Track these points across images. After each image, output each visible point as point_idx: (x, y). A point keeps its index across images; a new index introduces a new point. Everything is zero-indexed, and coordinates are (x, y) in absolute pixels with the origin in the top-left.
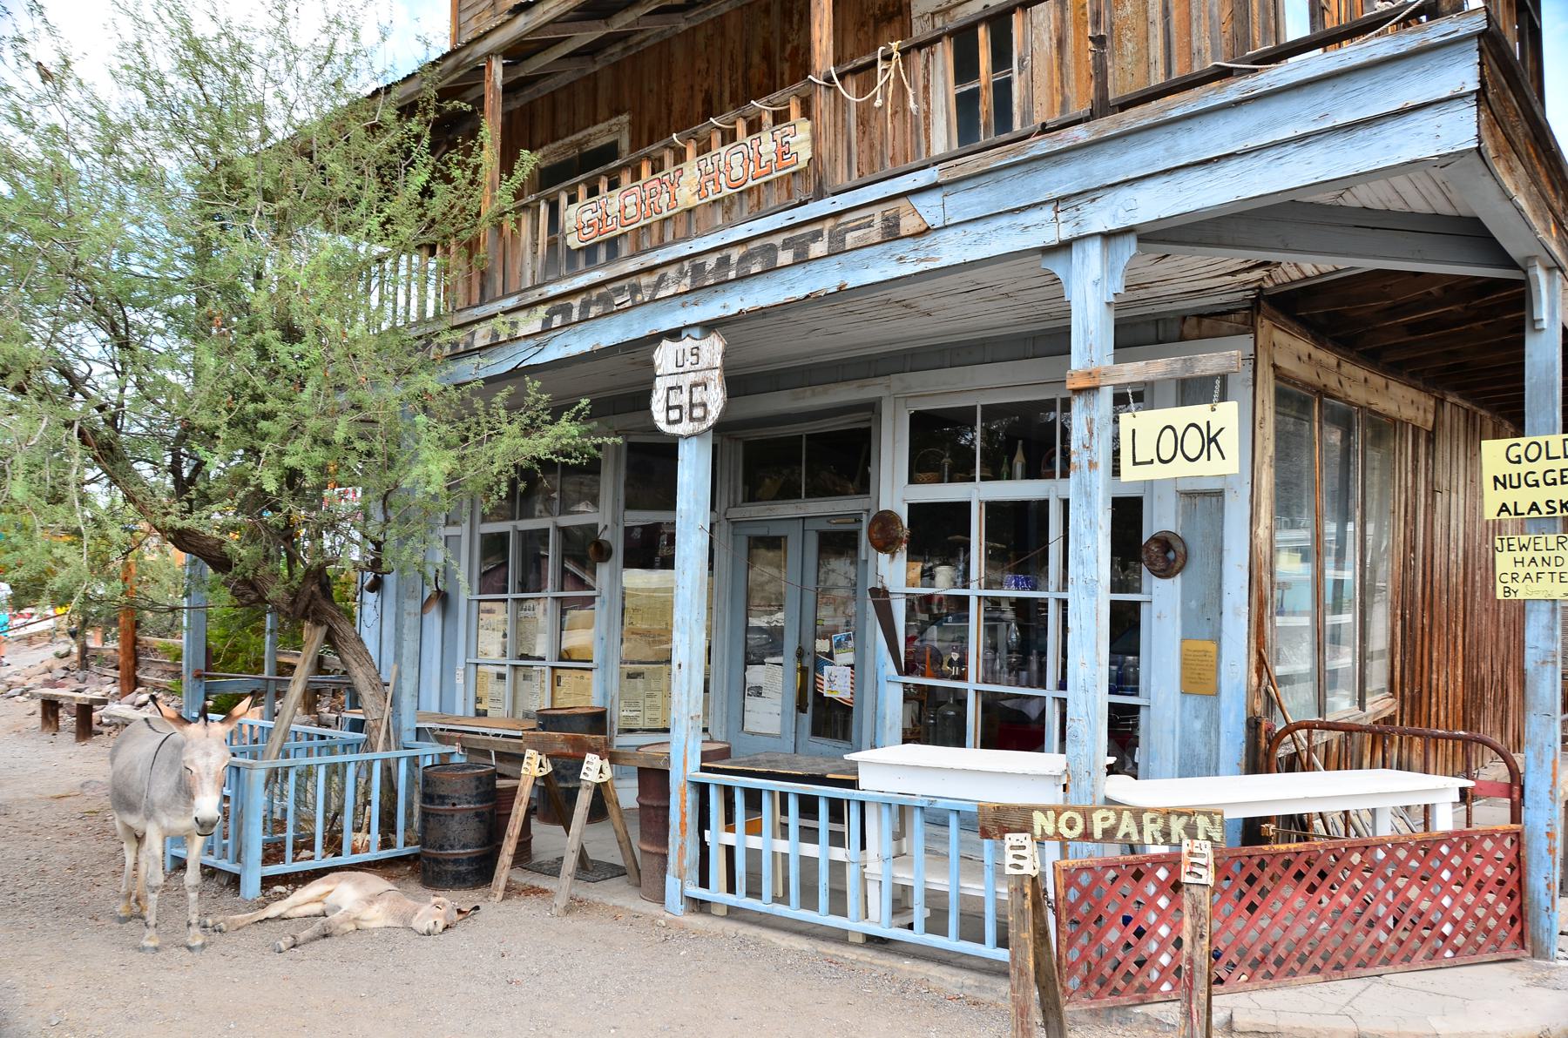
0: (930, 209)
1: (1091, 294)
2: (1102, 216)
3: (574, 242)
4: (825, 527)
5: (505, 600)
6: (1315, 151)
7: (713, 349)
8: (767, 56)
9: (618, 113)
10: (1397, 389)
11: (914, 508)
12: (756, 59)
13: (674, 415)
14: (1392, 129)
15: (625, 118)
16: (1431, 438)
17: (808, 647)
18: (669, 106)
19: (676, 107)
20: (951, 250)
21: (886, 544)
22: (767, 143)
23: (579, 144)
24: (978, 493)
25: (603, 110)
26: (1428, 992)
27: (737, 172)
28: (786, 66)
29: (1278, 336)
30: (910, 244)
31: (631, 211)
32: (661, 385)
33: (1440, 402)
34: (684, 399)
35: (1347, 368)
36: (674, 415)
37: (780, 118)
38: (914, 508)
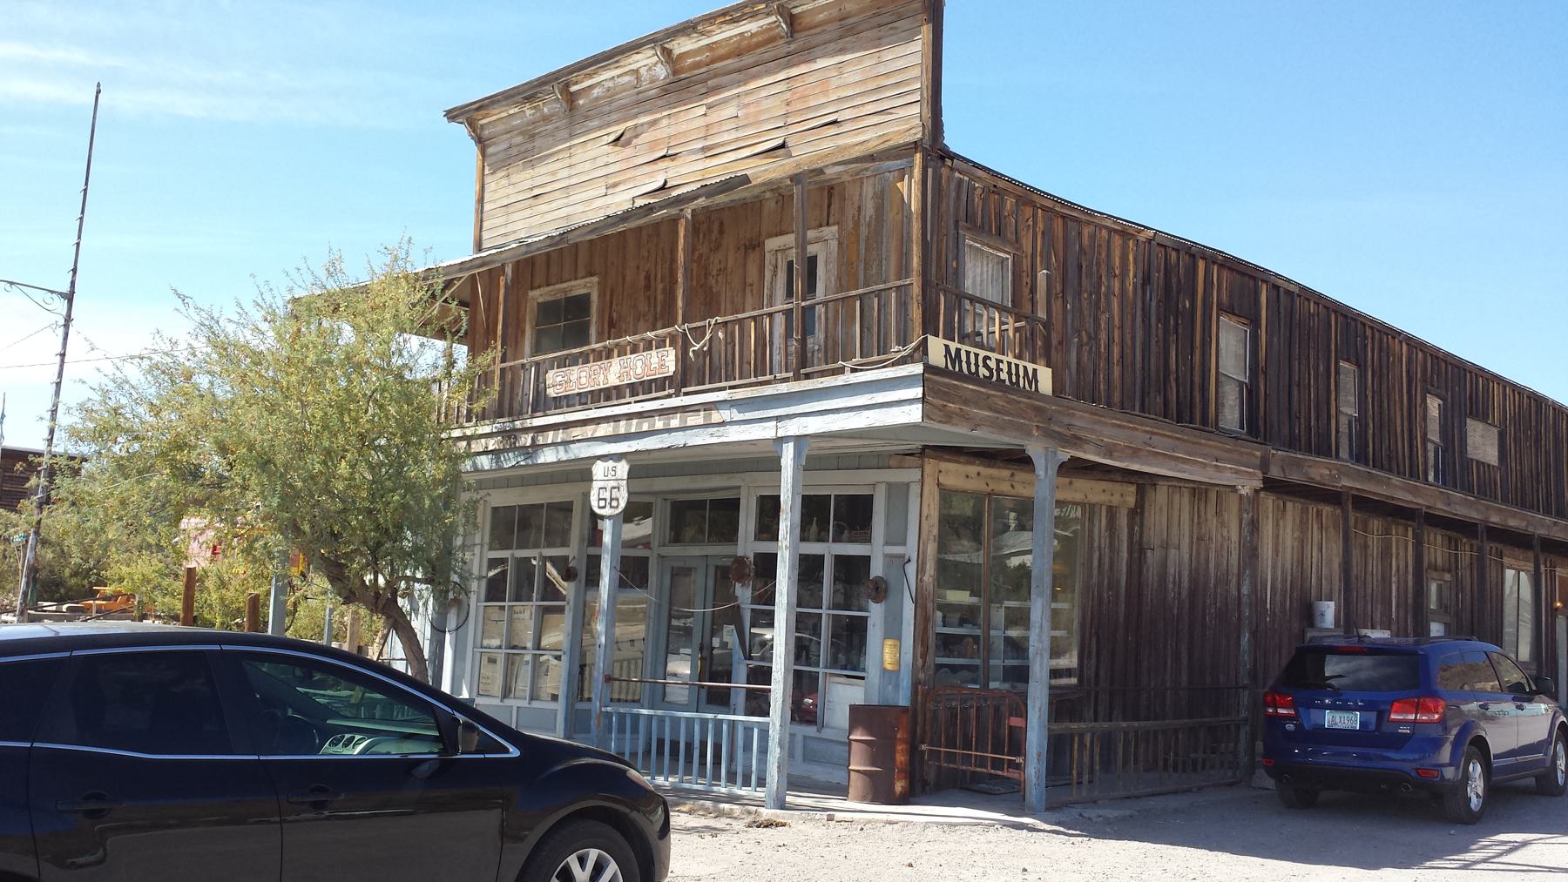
3: (551, 392)
4: (719, 563)
5: (502, 608)
7: (623, 468)
9: (591, 275)
11: (757, 555)
13: (602, 503)
14: (895, 410)
15: (595, 279)
19: (628, 279)
21: (741, 578)
23: (565, 291)
25: (581, 272)
26: (56, 406)
27: (639, 371)
31: (583, 380)
32: (596, 485)
34: (607, 495)
36: (602, 503)
38: (757, 555)
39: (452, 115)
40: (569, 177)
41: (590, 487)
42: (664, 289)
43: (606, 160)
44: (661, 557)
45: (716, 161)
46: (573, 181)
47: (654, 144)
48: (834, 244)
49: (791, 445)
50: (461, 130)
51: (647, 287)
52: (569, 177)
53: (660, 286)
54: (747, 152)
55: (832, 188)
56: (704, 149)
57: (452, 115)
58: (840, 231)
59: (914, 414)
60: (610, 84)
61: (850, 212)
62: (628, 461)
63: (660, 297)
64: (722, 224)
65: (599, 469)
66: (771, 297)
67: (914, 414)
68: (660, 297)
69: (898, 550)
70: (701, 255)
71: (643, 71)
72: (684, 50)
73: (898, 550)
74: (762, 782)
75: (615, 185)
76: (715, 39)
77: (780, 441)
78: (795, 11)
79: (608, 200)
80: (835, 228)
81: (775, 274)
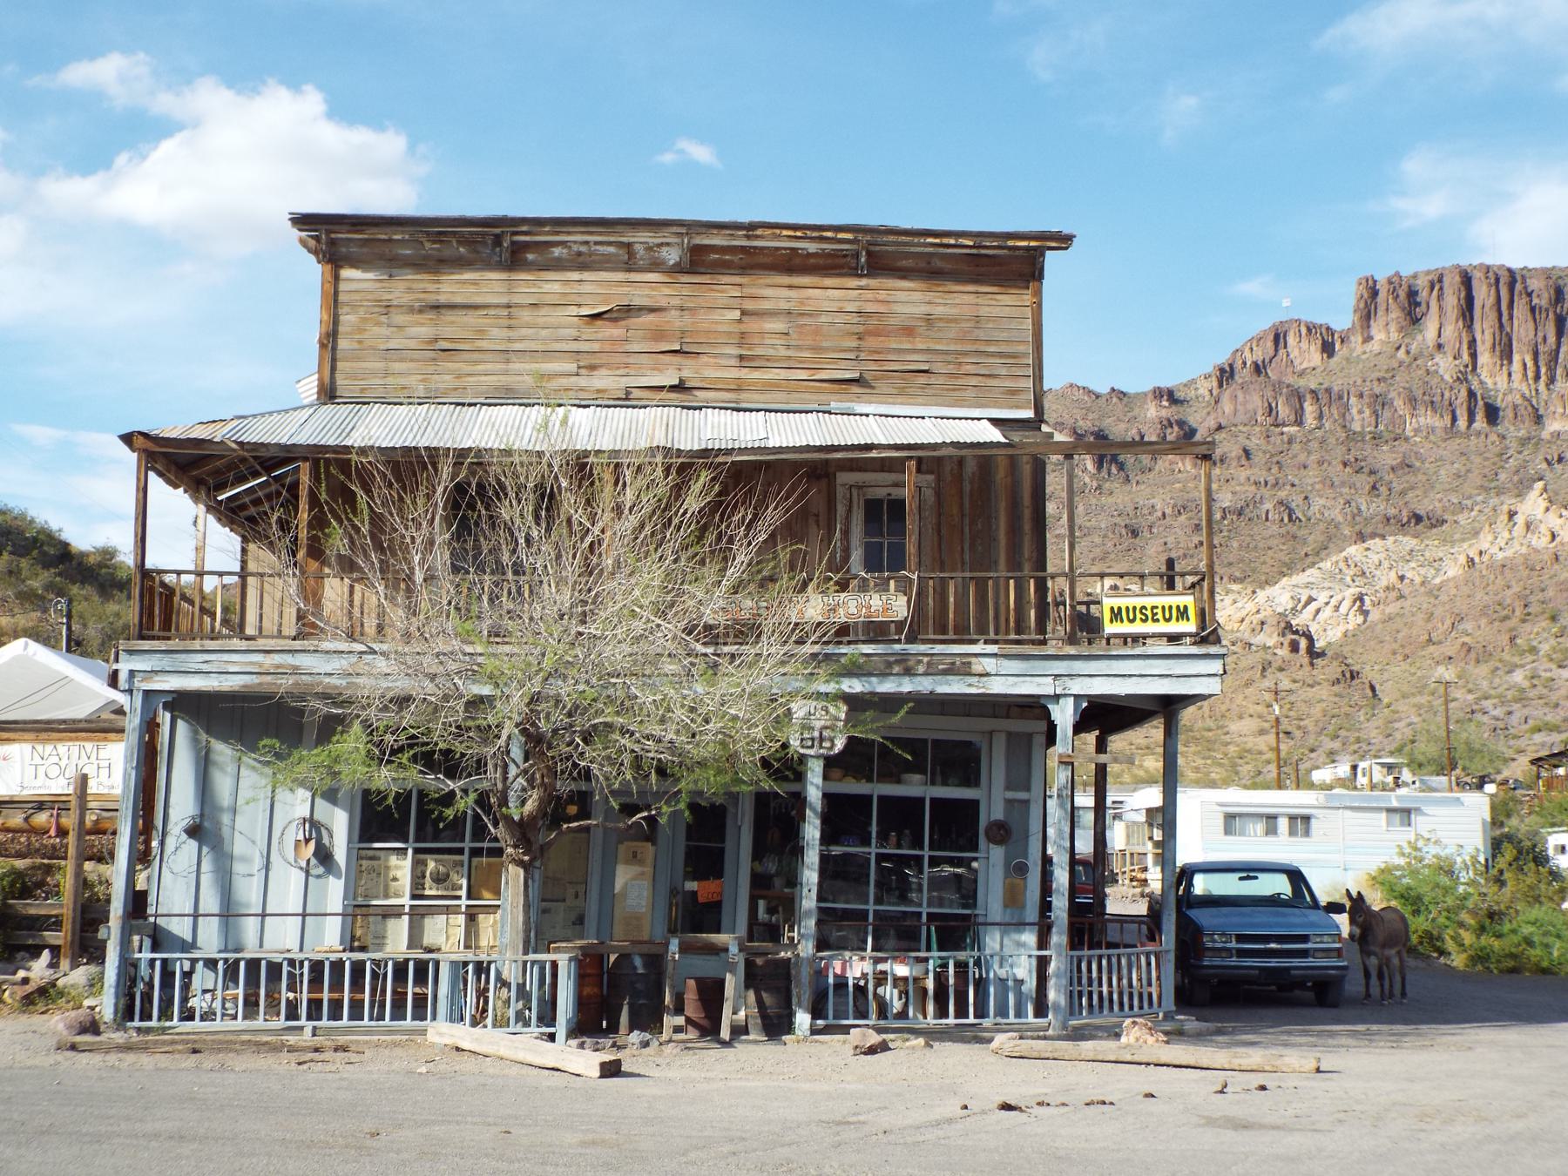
0: (989, 665)
20: (997, 687)
30: (976, 679)
39: (303, 221)
45: (756, 374)
46: (518, 346)
47: (659, 334)
54: (803, 375)
56: (741, 357)
58: (938, 480)
60: (583, 249)
69: (1022, 795)
73: (1022, 795)
75: (592, 368)
77: (1056, 698)
79: (582, 382)
80: (931, 477)
81: (850, 511)
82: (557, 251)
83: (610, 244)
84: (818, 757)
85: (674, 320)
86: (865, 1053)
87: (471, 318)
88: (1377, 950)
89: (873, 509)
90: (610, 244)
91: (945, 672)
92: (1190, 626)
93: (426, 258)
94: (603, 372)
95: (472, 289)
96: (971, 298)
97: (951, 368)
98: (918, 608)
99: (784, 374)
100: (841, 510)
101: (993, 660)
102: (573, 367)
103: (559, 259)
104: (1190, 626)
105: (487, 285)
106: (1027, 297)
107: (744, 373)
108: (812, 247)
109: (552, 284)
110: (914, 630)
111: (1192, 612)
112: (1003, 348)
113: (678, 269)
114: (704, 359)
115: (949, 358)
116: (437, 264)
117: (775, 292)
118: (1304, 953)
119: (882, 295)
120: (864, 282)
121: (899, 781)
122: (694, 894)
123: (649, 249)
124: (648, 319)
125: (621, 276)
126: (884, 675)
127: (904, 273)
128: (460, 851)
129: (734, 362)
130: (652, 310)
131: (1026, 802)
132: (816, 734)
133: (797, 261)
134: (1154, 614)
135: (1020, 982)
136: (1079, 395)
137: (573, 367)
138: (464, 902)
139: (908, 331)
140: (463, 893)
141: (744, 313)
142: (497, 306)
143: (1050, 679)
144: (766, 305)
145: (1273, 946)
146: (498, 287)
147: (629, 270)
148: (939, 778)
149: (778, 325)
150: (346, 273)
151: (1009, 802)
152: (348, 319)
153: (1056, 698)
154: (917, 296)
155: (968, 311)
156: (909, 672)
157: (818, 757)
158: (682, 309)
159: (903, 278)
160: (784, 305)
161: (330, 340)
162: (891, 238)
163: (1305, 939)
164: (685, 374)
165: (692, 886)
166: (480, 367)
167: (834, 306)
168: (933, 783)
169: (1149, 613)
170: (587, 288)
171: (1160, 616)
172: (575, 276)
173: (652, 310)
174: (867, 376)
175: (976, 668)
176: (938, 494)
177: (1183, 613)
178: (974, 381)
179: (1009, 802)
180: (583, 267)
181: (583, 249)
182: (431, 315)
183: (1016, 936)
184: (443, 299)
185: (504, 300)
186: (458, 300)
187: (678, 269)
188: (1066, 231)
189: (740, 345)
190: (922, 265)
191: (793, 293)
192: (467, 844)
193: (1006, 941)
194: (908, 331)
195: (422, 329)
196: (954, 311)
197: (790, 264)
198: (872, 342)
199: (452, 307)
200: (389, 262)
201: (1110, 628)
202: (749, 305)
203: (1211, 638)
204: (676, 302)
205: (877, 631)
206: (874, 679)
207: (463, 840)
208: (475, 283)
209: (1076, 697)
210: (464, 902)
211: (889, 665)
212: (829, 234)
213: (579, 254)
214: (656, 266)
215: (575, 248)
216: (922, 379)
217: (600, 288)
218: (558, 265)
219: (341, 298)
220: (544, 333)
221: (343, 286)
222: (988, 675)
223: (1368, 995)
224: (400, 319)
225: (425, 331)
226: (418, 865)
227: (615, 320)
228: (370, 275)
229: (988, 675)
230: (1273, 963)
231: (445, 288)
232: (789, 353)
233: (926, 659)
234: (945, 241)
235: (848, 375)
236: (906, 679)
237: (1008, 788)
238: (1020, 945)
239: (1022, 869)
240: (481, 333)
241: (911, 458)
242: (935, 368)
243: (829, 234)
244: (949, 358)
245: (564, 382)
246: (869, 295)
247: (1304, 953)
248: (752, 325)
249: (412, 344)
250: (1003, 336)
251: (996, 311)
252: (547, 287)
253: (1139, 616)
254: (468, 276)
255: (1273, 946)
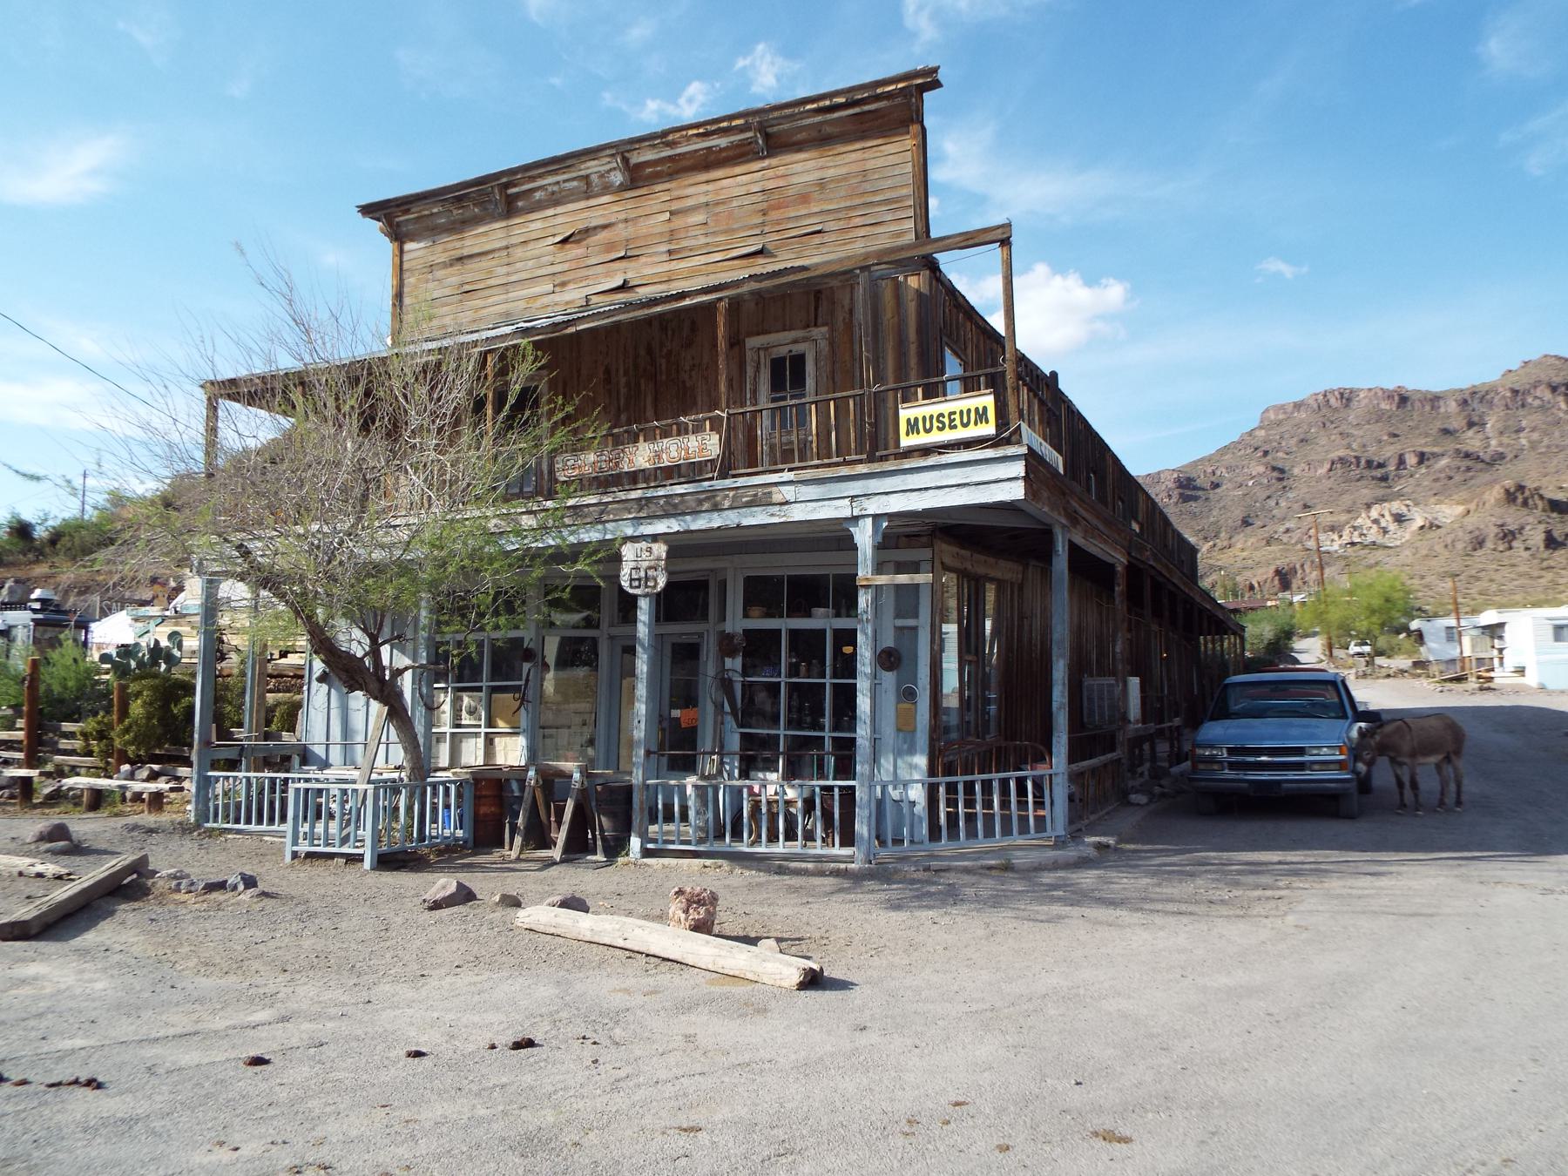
0: (788, 492)
1: (864, 536)
2: (874, 506)
6: (964, 490)
7: (660, 549)
8: (650, 351)
10: (1002, 563)
12: (642, 352)
16: (1021, 587)
17: (666, 714)
18: (579, 371)
20: (798, 514)
22: (693, 442)
24: (785, 624)
28: (663, 361)
29: (945, 546)
30: (777, 508)
33: (1026, 566)
35: (977, 556)
37: (698, 429)
39: (368, 210)
40: (508, 274)
41: (619, 569)
42: (628, 384)
43: (550, 258)
44: (612, 638)
45: (683, 264)
46: (514, 278)
47: (610, 247)
48: (824, 345)
49: (870, 520)
50: (374, 227)
51: (608, 380)
52: (508, 274)
53: (623, 380)
54: (718, 257)
55: (819, 292)
56: (670, 252)
57: (368, 210)
58: (832, 330)
59: (1017, 492)
60: (555, 188)
61: (840, 316)
62: (666, 542)
63: (623, 391)
64: (693, 323)
65: (628, 552)
66: (754, 392)
67: (1017, 492)
68: (623, 391)
69: (910, 622)
70: (670, 352)
71: (594, 178)
72: (642, 159)
73: (910, 622)
74: (298, 790)
75: (563, 284)
76: (679, 151)
77: (855, 519)
78: (770, 130)
79: (557, 298)
80: (824, 329)
81: (757, 369)
82: (538, 195)
83: (574, 179)
84: (645, 596)
85: (621, 232)
86: (431, 909)
87: (484, 263)
88: (1406, 760)
89: (777, 365)
90: (574, 179)
91: (749, 505)
92: (989, 429)
93: (454, 222)
94: (571, 286)
95: (484, 239)
96: (859, 155)
97: (842, 224)
98: (727, 445)
99: (704, 259)
100: (750, 371)
101: (791, 488)
102: (550, 287)
103: (539, 201)
104: (989, 429)
105: (489, 235)
106: (908, 142)
107: (674, 265)
108: (723, 142)
109: (533, 224)
110: (725, 467)
111: (991, 414)
112: (888, 195)
113: (623, 188)
114: (643, 259)
115: (841, 215)
116: (459, 226)
117: (696, 189)
118: (1300, 766)
119: (781, 171)
120: (766, 163)
121: (809, 615)
122: (678, 719)
123: (602, 176)
124: (602, 236)
125: (583, 204)
126: (695, 513)
127: (798, 147)
128: (479, 689)
129: (665, 257)
130: (605, 227)
131: (915, 629)
132: (642, 574)
133: (712, 157)
134: (951, 421)
135: (913, 803)
136: (1552, 361)
137: (550, 287)
138: (483, 730)
139: (804, 198)
140: (483, 723)
141: (672, 213)
142: (500, 249)
143: (847, 501)
144: (690, 202)
145: (1264, 758)
146: (500, 234)
147: (588, 198)
148: (843, 611)
149: (699, 218)
150: (408, 246)
151: (899, 629)
152: (410, 280)
153: (855, 519)
154: (812, 164)
155: (854, 168)
156: (716, 508)
157: (645, 596)
158: (626, 221)
159: (799, 151)
160: (703, 199)
161: (399, 296)
162: (776, 114)
163: (1300, 751)
164: (629, 275)
165: (676, 713)
166: (490, 300)
167: (743, 191)
168: (838, 615)
169: (946, 420)
170: (560, 220)
171: (957, 422)
172: (550, 212)
173: (605, 227)
174: (769, 247)
175: (777, 498)
176: (832, 343)
177: (981, 416)
178: (862, 232)
179: (899, 629)
180: (557, 203)
181: (555, 188)
182: (457, 267)
183: (909, 759)
184: (466, 252)
185: (504, 243)
186: (476, 250)
187: (623, 188)
188: (932, 65)
189: (670, 242)
190: (814, 134)
191: (710, 187)
192: (484, 684)
193: (900, 762)
194: (804, 198)
195: (453, 277)
196: (843, 171)
197: (708, 162)
198: (775, 215)
199: (471, 256)
200: (431, 230)
201: (906, 441)
202: (675, 206)
203: (1014, 439)
204: (622, 216)
205: (691, 471)
206: (688, 518)
207: (779, 675)
208: (484, 234)
209: (876, 517)
210: (483, 730)
211: (700, 502)
212: (725, 124)
213: (553, 193)
214: (607, 189)
215: (550, 189)
216: (817, 239)
217: (566, 218)
218: (540, 206)
219: (406, 266)
220: (530, 263)
221: (406, 258)
222: (787, 503)
223: (1442, 803)
224: (440, 274)
225: (455, 280)
226: (456, 702)
227: (578, 242)
228: (422, 245)
229: (787, 503)
230: (1265, 776)
231: (467, 242)
232: (709, 240)
233: (731, 494)
234: (821, 104)
235: (753, 249)
236: (716, 515)
237: (898, 616)
238: (913, 767)
239: (909, 695)
240: (490, 274)
241: (720, 299)
242: (827, 227)
243: (725, 124)
244: (841, 215)
245: (546, 300)
246: (770, 173)
247: (1300, 766)
248: (678, 222)
249: (447, 292)
250: (889, 183)
251: (880, 163)
252: (533, 226)
253: (935, 424)
254: (482, 229)
255: (1264, 758)
